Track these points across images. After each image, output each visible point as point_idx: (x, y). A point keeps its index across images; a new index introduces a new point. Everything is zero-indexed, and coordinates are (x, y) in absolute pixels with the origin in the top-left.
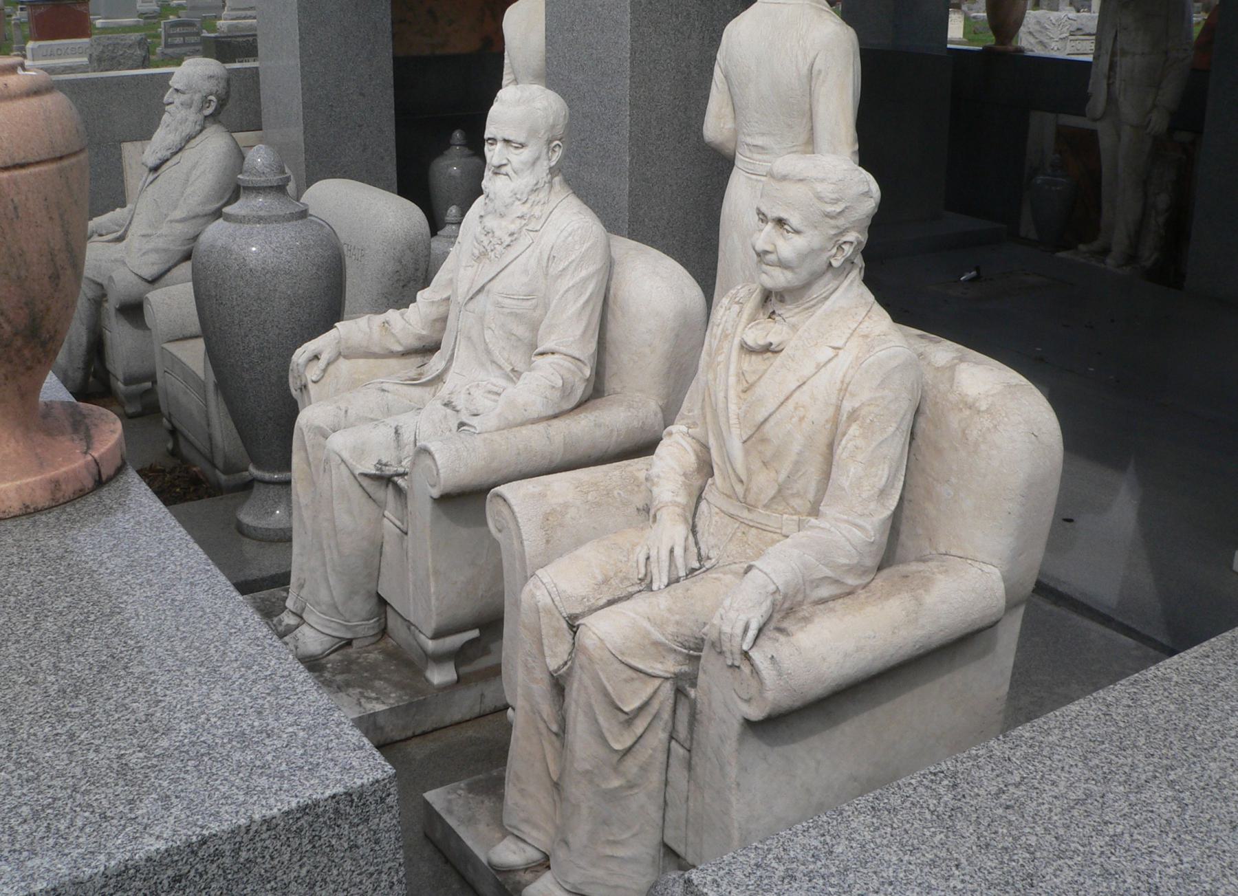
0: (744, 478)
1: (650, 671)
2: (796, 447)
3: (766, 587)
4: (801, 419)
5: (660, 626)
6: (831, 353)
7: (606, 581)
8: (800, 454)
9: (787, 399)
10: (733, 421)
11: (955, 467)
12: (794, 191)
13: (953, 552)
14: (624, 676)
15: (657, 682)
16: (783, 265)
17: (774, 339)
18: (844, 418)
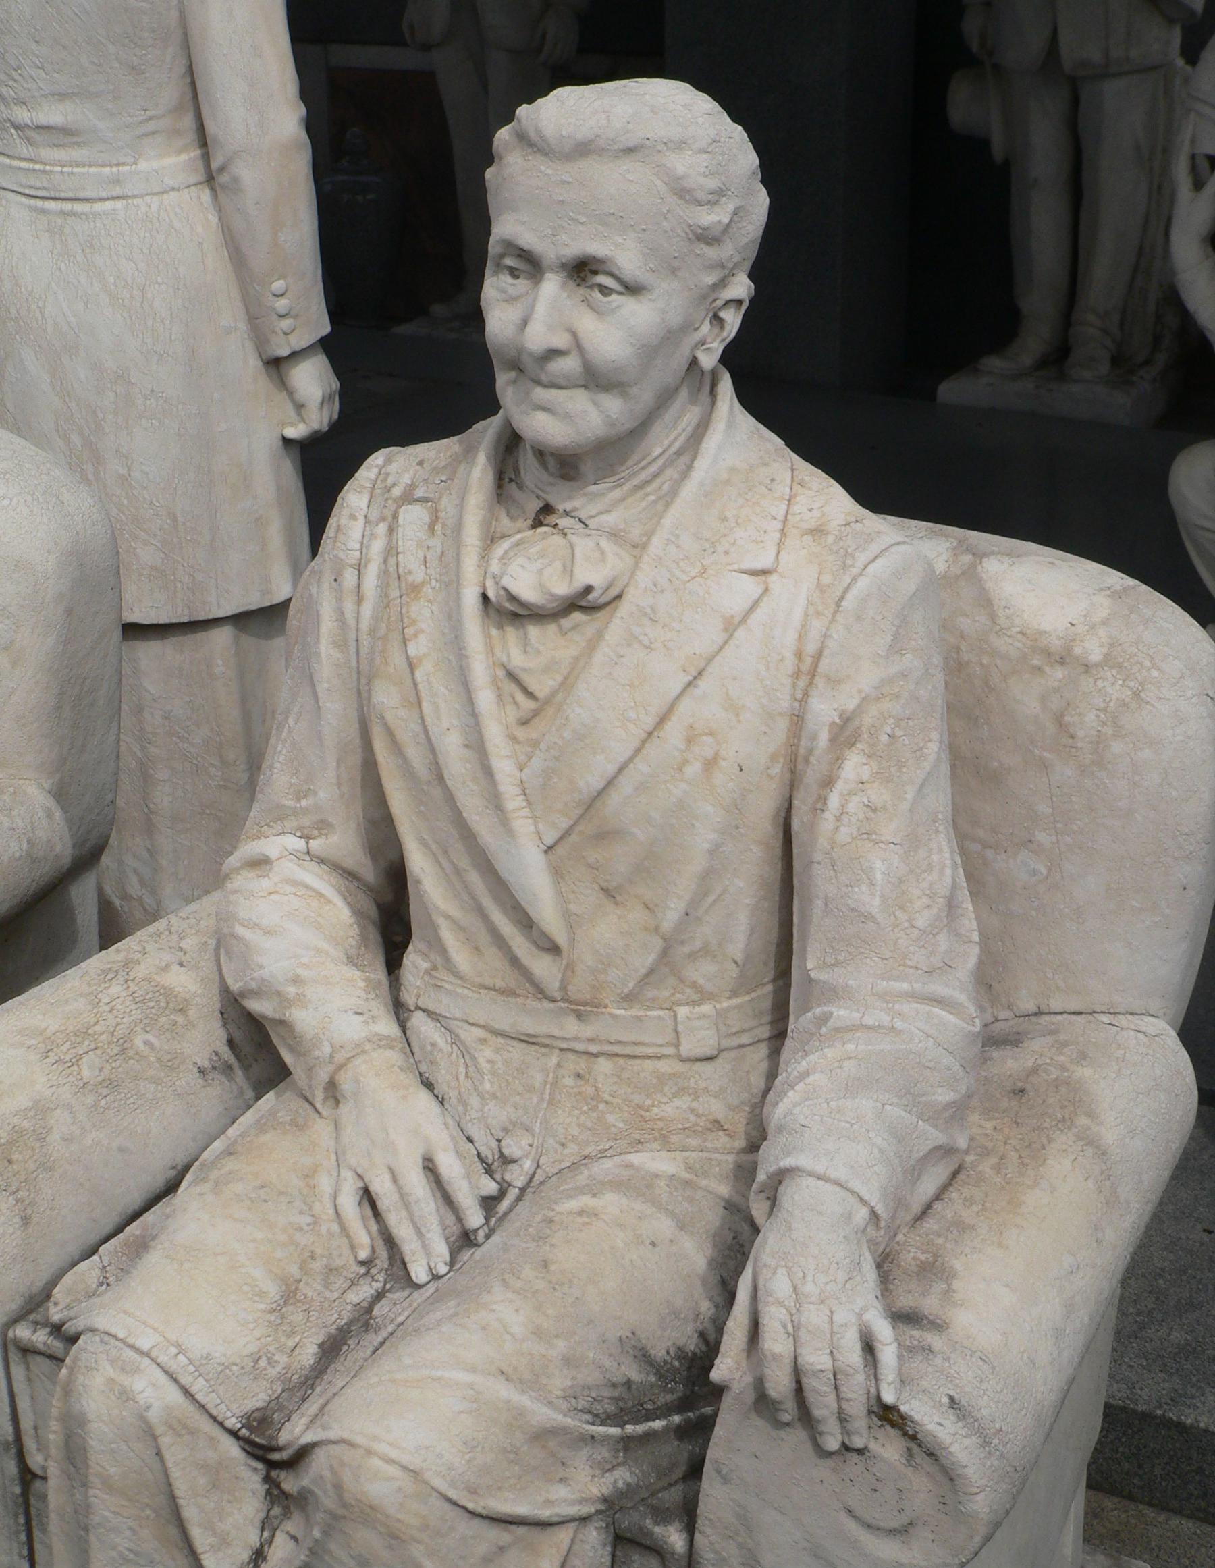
0: (561, 939)
1: (545, 1514)
2: (703, 838)
3: (848, 1217)
4: (710, 764)
5: (531, 1382)
6: (751, 587)
7: (290, 1295)
8: (713, 852)
9: (662, 720)
10: (513, 801)
11: (1043, 808)
12: (617, 180)
13: (1056, 1004)
14: (482, 1549)
15: (563, 1536)
16: (596, 379)
17: (592, 574)
18: (824, 738)
